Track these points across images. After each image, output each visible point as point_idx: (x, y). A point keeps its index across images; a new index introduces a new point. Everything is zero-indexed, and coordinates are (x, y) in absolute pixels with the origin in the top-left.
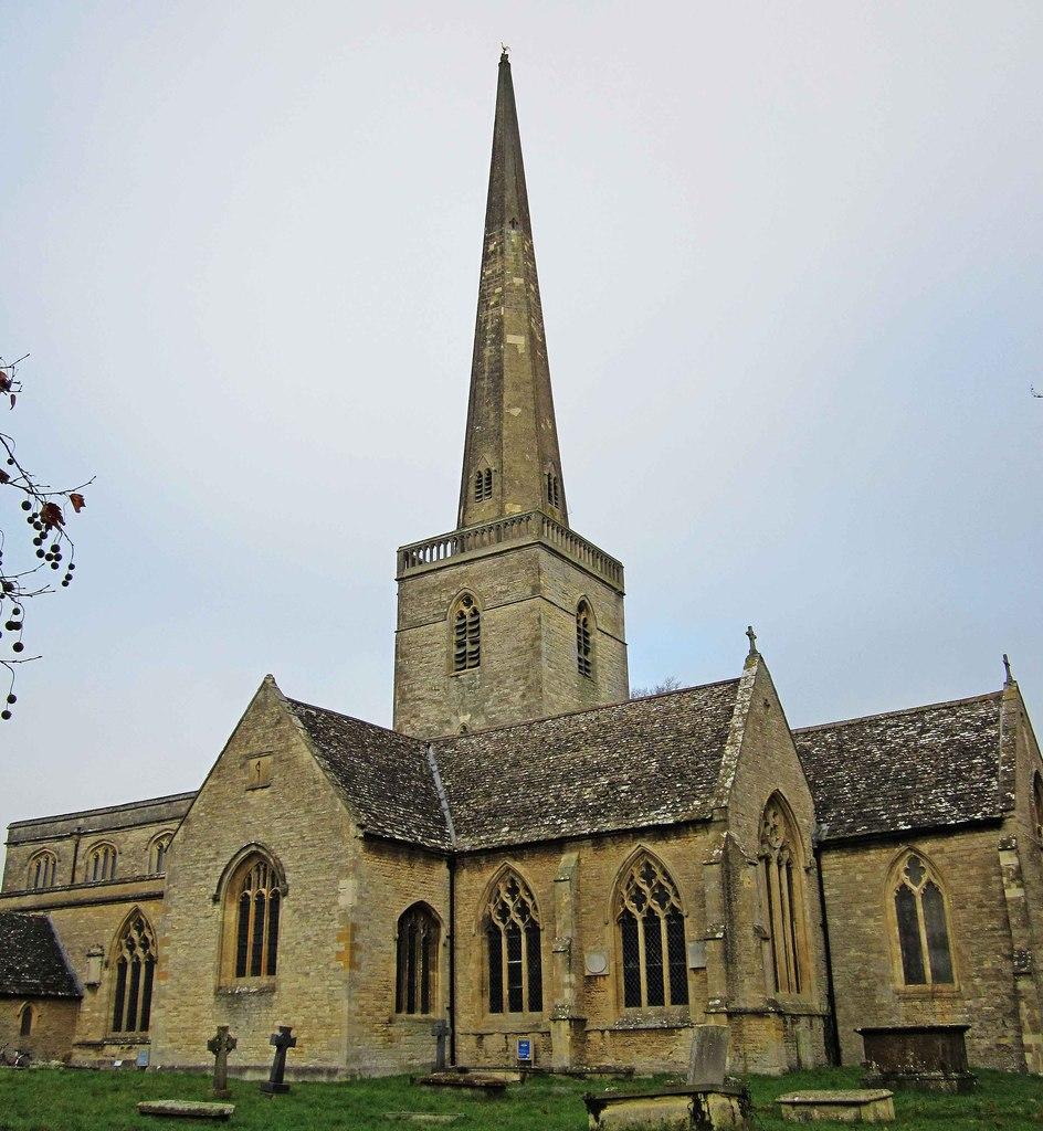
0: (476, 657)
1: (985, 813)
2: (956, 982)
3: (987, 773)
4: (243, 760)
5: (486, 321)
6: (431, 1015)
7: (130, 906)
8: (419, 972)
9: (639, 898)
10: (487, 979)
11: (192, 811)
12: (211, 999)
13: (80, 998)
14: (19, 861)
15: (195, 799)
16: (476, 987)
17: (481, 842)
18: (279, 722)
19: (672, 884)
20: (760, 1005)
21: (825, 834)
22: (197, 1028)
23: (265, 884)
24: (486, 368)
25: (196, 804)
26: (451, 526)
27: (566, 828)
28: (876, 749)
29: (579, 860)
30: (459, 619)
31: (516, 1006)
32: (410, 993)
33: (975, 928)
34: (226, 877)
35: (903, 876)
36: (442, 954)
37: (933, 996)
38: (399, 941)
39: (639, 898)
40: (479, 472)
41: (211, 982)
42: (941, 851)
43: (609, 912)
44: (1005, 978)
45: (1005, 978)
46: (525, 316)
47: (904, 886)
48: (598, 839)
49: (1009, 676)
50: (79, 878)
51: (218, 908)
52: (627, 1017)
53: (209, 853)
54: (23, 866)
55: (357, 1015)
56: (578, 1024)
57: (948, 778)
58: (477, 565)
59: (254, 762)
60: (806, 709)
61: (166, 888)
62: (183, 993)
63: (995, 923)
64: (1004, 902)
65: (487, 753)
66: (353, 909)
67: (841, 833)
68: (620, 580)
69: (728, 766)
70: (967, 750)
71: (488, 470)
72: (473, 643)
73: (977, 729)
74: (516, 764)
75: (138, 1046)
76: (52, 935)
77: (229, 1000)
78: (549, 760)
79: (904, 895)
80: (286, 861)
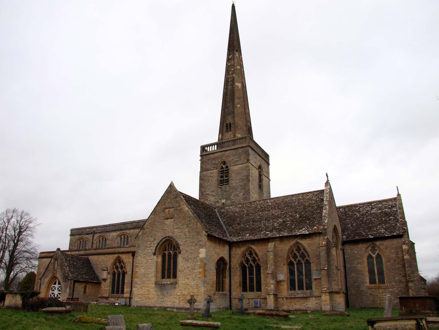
0: (227, 181)
1: (397, 233)
2: (386, 284)
3: (395, 221)
4: (163, 210)
5: (229, 78)
6: (224, 292)
7: (117, 255)
8: (221, 279)
9: (295, 257)
10: (242, 281)
11: (145, 225)
12: (154, 286)
13: (100, 283)
14: (74, 241)
15: (146, 222)
16: (238, 284)
17: (240, 239)
18: (176, 197)
19: (307, 253)
20: (338, 290)
21: (345, 239)
22: (149, 294)
23: (171, 248)
24: (229, 92)
25: (146, 223)
26: (216, 140)
27: (270, 235)
28: (357, 214)
29: (275, 245)
30: (221, 169)
31: (252, 290)
32: (220, 286)
33: (393, 267)
34: (158, 247)
35: (370, 252)
36: (227, 273)
37: (379, 288)
38: (216, 269)
39: (295, 257)
40: (227, 124)
41: (153, 280)
42: (383, 244)
43: (285, 261)
44: (402, 282)
45: (402, 282)
46: (241, 78)
47: (370, 255)
48: (282, 239)
49: (398, 193)
50: (94, 246)
51: (155, 257)
52: (291, 294)
53: (152, 239)
54: (75, 242)
55: (206, 292)
56: (275, 295)
57: (383, 222)
58: (228, 152)
59: (167, 210)
60: (340, 202)
61: (136, 250)
62: (143, 283)
63: (399, 266)
64: (403, 259)
65: (236, 211)
66: (205, 258)
67: (350, 238)
68: (268, 160)
69: (325, 216)
70: (386, 214)
71: (230, 123)
72: (226, 177)
73: (389, 208)
74: (247, 215)
75: (120, 299)
76: (91, 263)
77: (160, 286)
78: (259, 214)
79: (370, 257)
80: (179, 242)
